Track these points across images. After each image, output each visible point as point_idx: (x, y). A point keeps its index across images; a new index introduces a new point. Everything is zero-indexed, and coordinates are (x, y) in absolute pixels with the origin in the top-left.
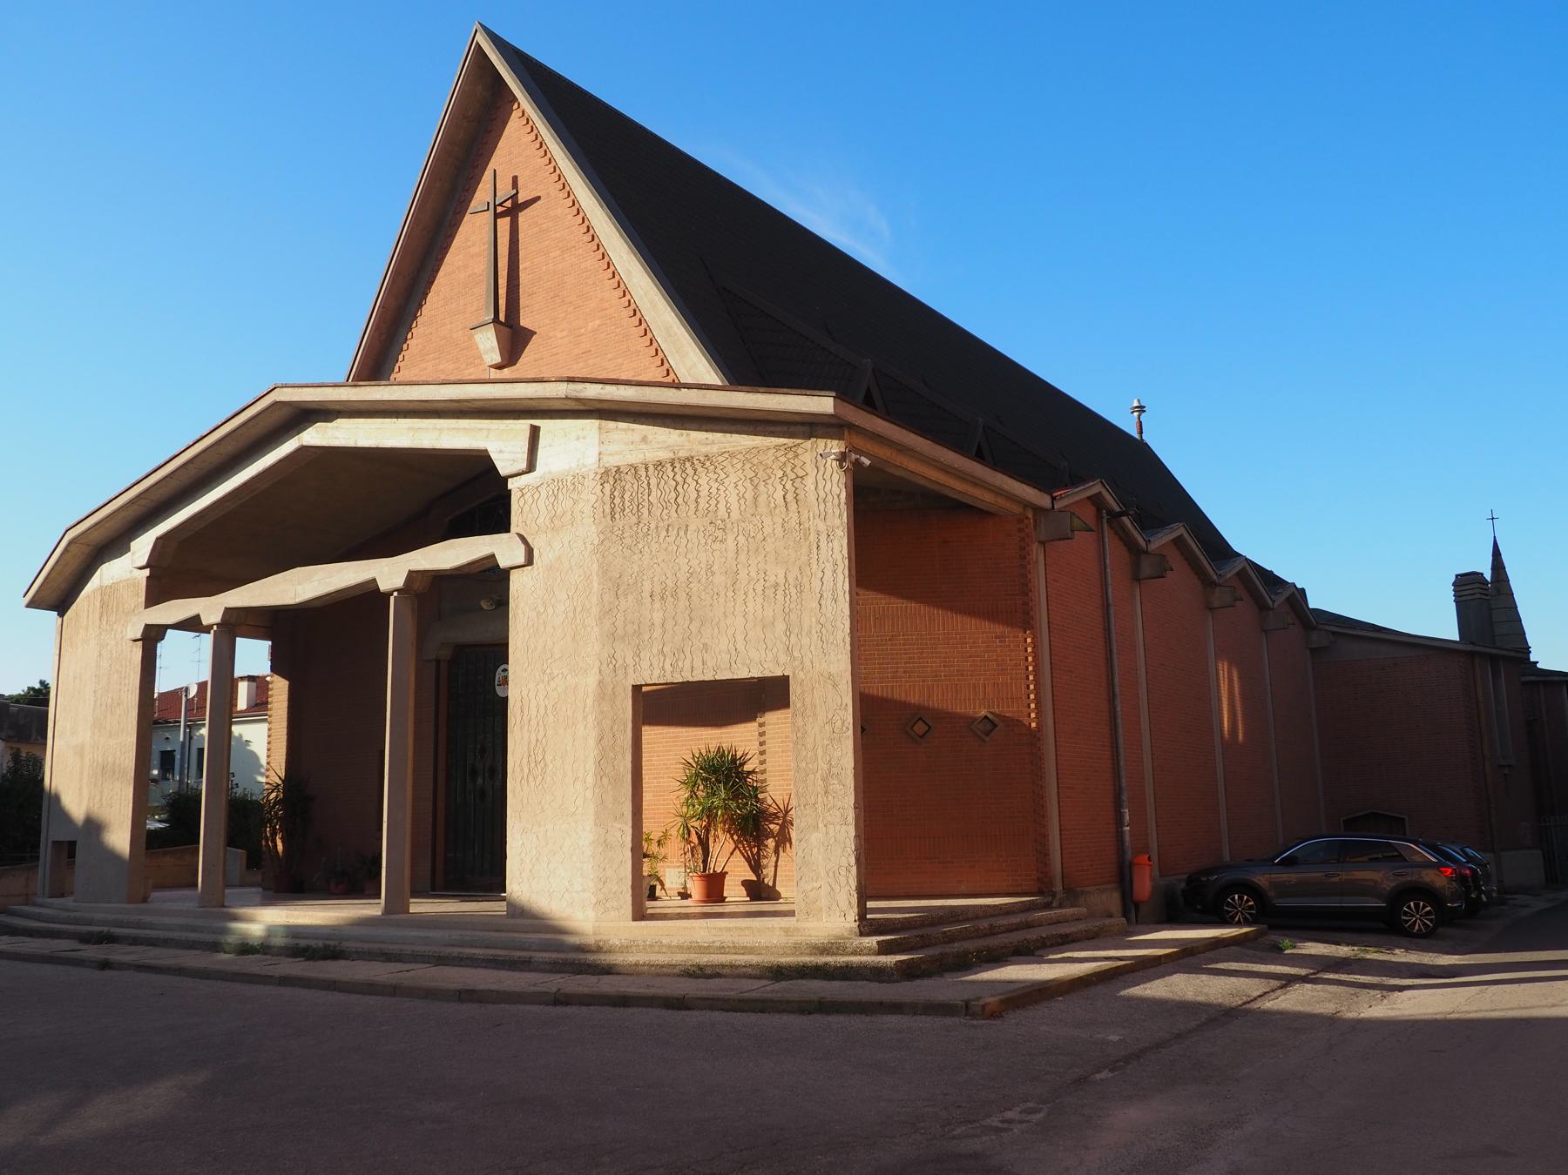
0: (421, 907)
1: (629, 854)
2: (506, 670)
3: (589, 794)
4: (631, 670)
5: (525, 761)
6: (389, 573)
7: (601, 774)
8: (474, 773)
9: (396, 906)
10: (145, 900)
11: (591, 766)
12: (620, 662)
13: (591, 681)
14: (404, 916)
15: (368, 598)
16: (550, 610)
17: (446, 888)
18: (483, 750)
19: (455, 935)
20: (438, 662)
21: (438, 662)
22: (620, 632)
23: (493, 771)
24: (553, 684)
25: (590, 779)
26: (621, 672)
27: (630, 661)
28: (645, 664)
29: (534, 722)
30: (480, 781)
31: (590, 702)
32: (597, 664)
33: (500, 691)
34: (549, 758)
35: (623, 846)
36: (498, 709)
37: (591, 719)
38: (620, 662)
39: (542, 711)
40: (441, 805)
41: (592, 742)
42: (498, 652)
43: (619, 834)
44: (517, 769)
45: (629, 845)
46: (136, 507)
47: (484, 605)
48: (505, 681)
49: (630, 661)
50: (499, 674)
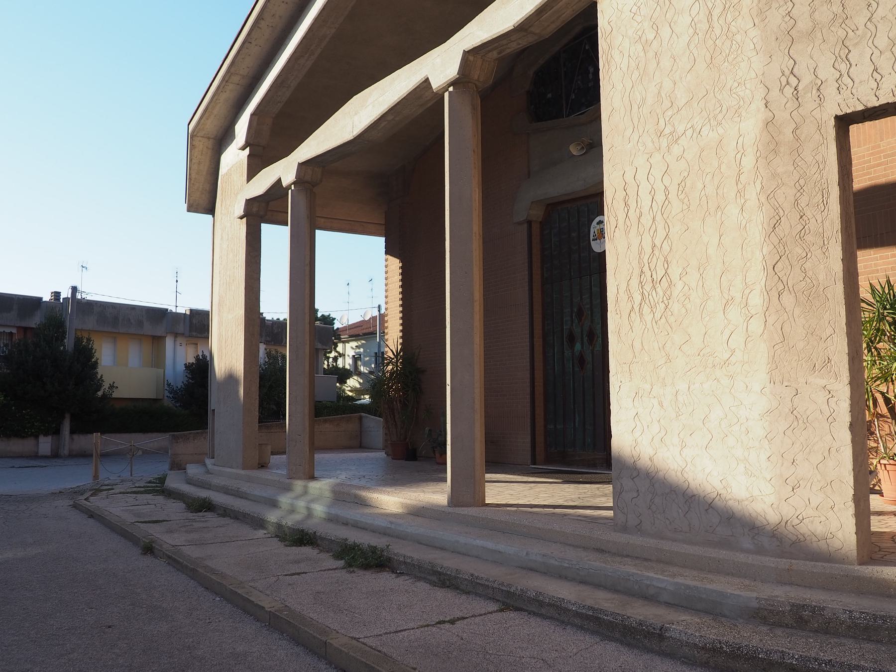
0: (505, 491)
1: (847, 436)
2: (601, 222)
3: (756, 326)
4: (830, 91)
5: (635, 283)
6: (440, 66)
7: (778, 286)
8: (572, 339)
9: (467, 494)
10: (263, 466)
11: (757, 275)
12: (807, 79)
13: (751, 126)
14: (855, 246)
15: (423, 104)
16: (665, 32)
17: (548, 460)
18: (580, 314)
19: (536, 551)
20: (529, 223)
21: (529, 223)
22: (804, 24)
23: (591, 335)
24: (676, 150)
25: (757, 300)
26: (809, 100)
27: (827, 73)
28: (861, 71)
29: (647, 220)
30: (578, 346)
31: (748, 162)
32: (762, 92)
33: (596, 247)
34: (675, 271)
35: (831, 419)
36: (598, 264)
37: (752, 193)
38: (807, 79)
39: (660, 197)
40: (539, 375)
41: (756, 231)
42: (592, 202)
43: (821, 397)
44: (623, 296)
45: (847, 418)
46: (231, 86)
47: (574, 150)
48: (601, 234)
49: (827, 73)
50: (594, 228)
